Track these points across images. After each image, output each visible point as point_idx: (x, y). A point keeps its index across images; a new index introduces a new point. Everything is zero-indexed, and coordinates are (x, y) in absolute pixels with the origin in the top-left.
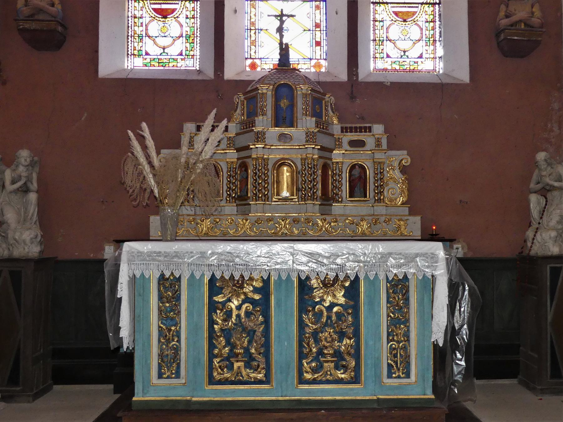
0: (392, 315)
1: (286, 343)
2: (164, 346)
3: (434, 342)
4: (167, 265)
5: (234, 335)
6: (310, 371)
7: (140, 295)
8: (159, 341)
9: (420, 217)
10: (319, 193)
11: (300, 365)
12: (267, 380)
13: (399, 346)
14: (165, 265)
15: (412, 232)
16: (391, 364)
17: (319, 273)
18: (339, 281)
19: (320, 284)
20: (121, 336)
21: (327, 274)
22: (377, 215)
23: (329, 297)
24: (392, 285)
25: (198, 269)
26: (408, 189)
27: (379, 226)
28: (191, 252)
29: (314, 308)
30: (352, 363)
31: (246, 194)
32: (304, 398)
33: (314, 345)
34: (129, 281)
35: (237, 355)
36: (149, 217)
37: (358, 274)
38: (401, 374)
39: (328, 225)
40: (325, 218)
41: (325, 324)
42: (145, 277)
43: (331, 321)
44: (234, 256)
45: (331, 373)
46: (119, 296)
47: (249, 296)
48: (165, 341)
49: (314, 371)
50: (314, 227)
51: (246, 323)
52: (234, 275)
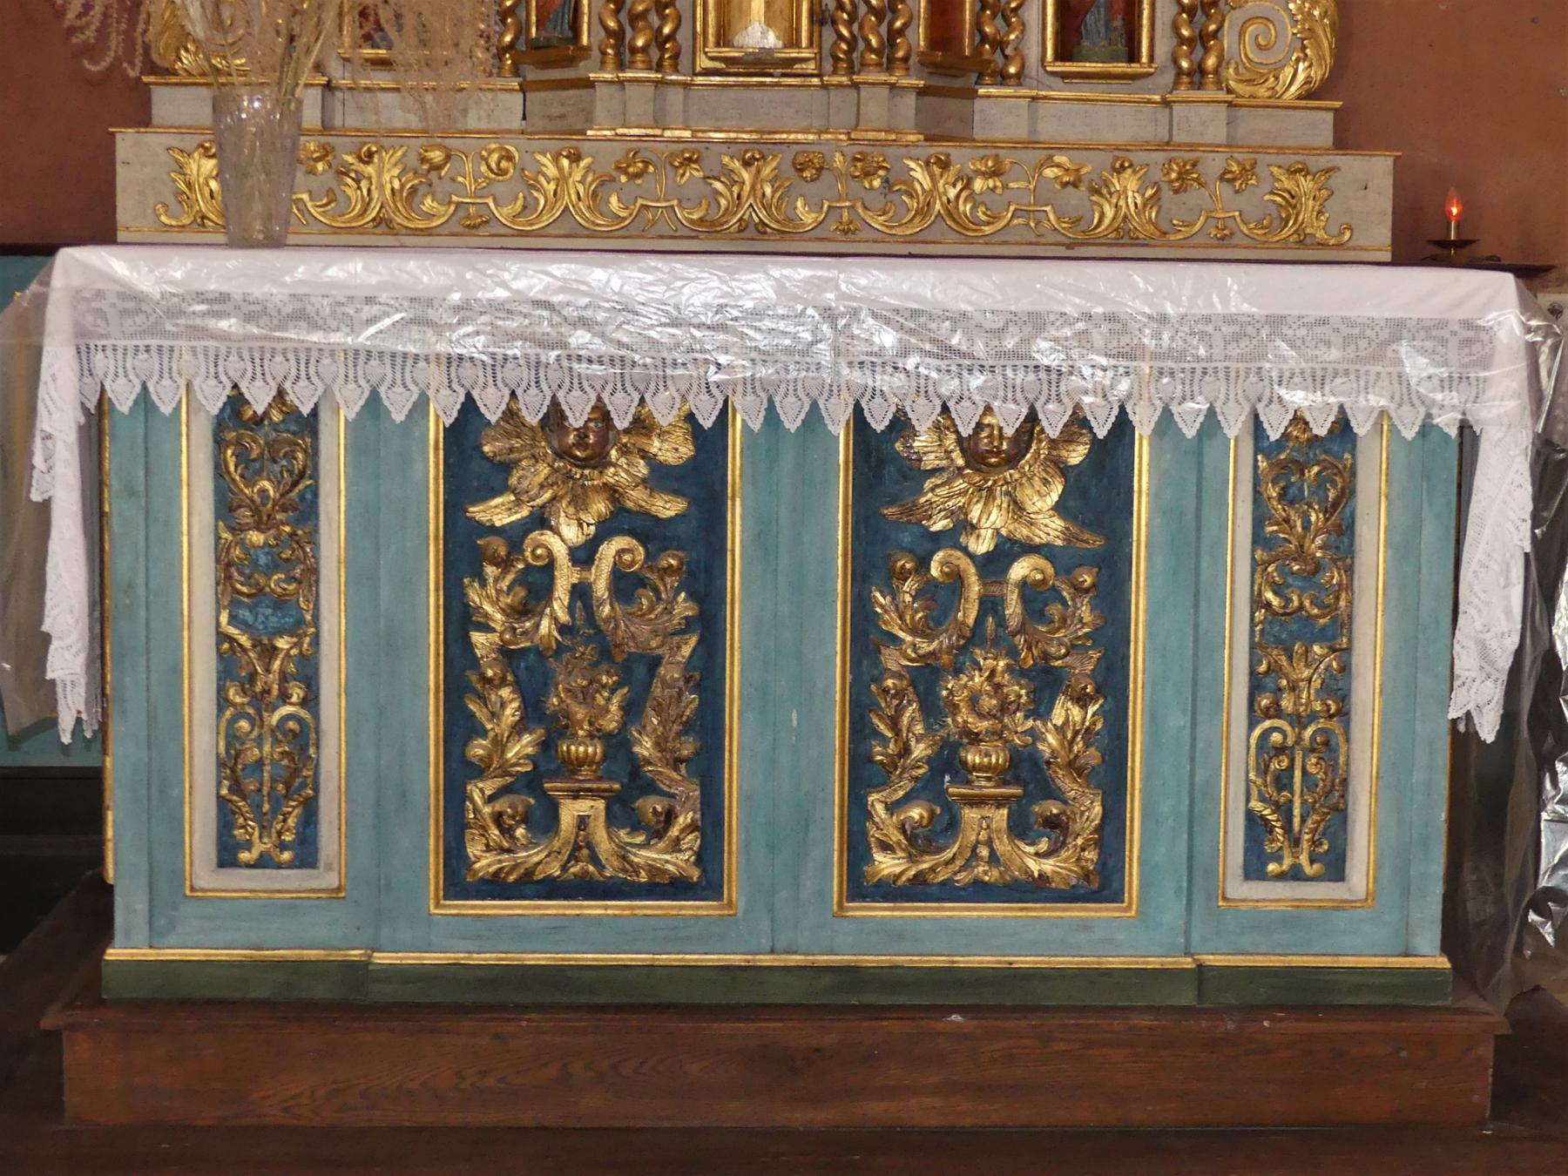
0: (1275, 602)
1: (794, 715)
2: (244, 725)
3: (1454, 722)
4: (257, 355)
5: (561, 678)
6: (899, 843)
7: (132, 493)
8: (222, 702)
9: (1390, 162)
10: (919, 37)
11: (857, 813)
12: (706, 884)
13: (1299, 739)
14: (246, 356)
15: (1350, 228)
16: (1263, 818)
17: (951, 404)
18: (1040, 441)
19: (954, 455)
20: (49, 676)
21: (988, 410)
22: (1192, 147)
23: (995, 511)
24: (1283, 466)
25: (398, 376)
26: (1332, 25)
27: (1195, 196)
28: (369, 300)
29: (923, 563)
30: (1089, 809)
31: (570, 34)
32: (870, 960)
33: (919, 728)
34: (81, 428)
35: (571, 767)
36: (113, 134)
37: (1129, 410)
38: (1304, 859)
39: (959, 186)
40: (948, 155)
41: (974, 630)
42: (156, 408)
43: (1001, 622)
44: (566, 319)
45: (993, 852)
46: (36, 497)
47: (630, 505)
48: (245, 700)
49: (919, 841)
50: (890, 196)
51: (617, 626)
52: (564, 407)
